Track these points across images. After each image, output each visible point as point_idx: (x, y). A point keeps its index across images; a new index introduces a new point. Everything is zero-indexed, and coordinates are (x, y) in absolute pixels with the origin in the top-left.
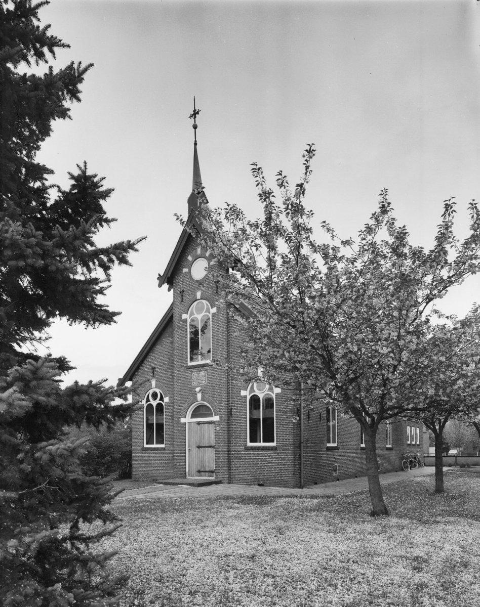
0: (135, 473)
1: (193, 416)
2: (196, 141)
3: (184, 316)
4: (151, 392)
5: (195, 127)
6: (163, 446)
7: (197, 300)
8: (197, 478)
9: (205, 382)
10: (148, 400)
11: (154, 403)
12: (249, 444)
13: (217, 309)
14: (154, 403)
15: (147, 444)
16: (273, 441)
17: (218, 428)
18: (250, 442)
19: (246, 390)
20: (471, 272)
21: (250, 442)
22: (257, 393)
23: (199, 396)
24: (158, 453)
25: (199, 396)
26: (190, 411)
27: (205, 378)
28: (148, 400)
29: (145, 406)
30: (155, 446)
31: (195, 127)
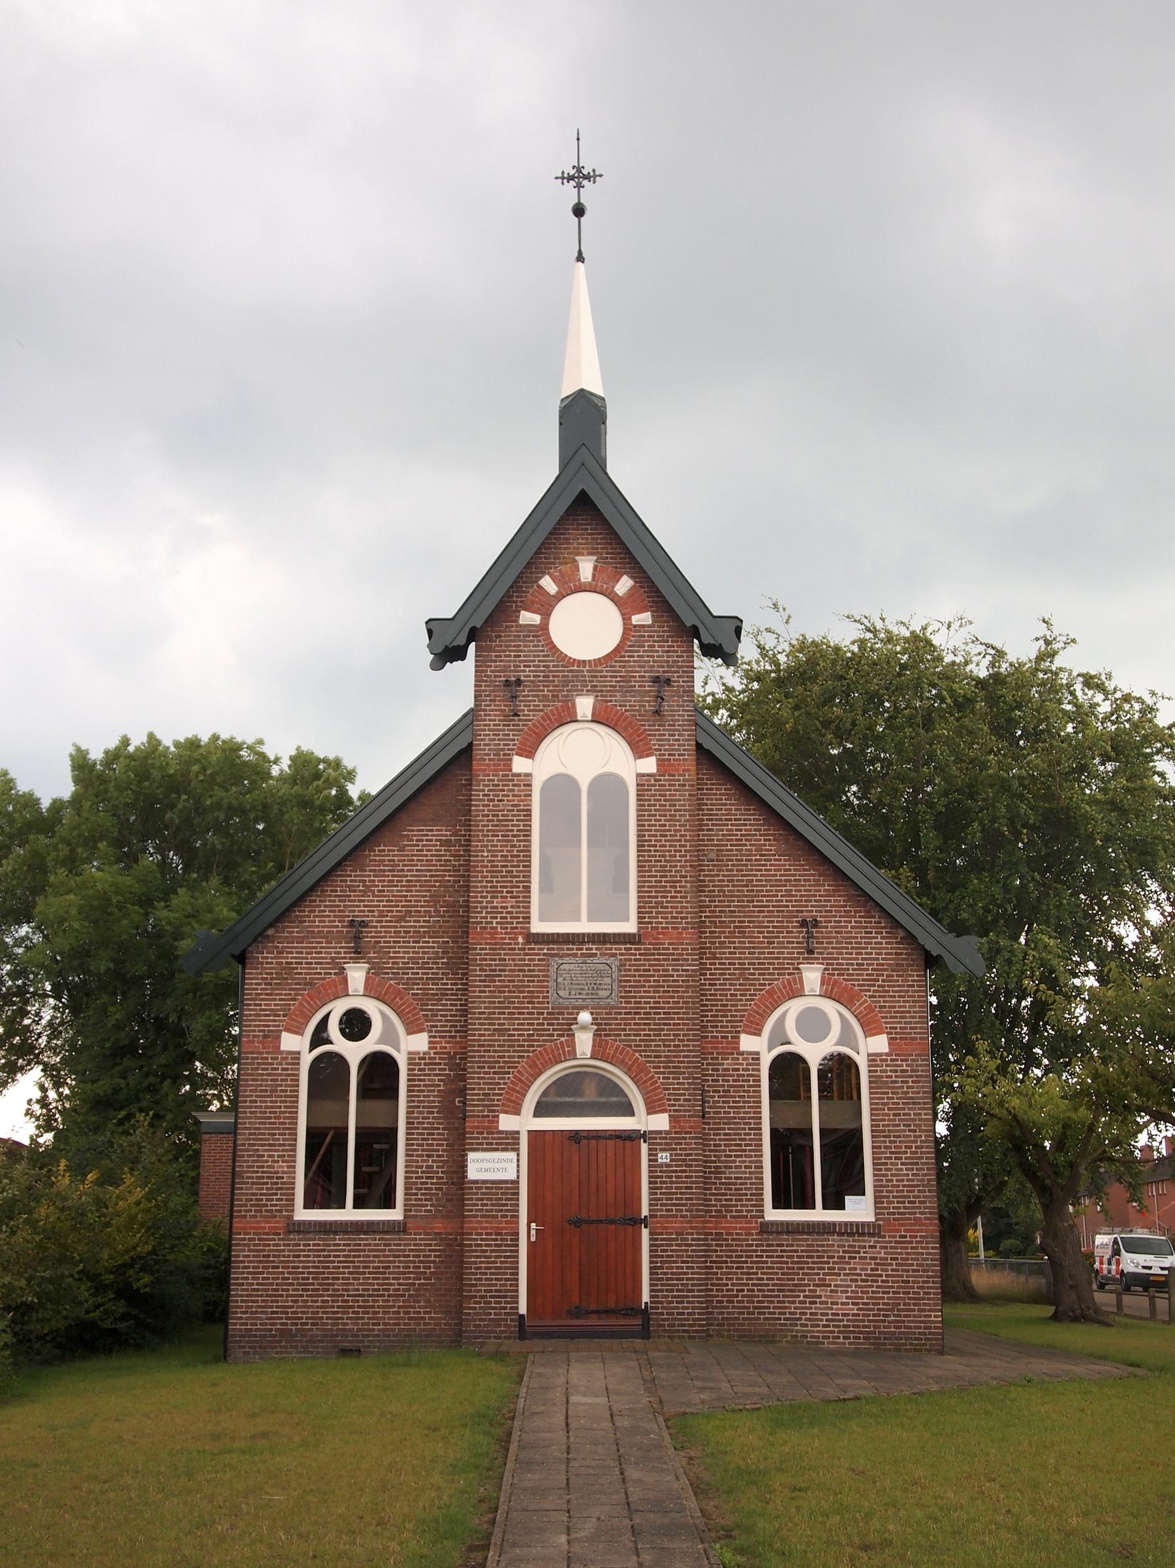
0: (239, 1321)
1: (541, 1110)
2: (580, 252)
3: (520, 764)
4: (338, 1009)
5: (579, 211)
6: (394, 1215)
7: (577, 721)
8: (568, 1322)
9: (609, 993)
10: (320, 1037)
11: (354, 1052)
12: (774, 1215)
13: (658, 765)
14: (354, 1052)
15: (308, 1205)
16: (389, 1203)
17: (664, 1157)
18: (305, 1207)
19: (758, 1033)
20: (1051, 1310)
21: (305, 1207)
22: (800, 1046)
23: (584, 1042)
24: (374, 1240)
25: (584, 1042)
26: (534, 1094)
27: (608, 981)
28: (320, 1037)
29: (307, 1059)
30: (349, 1214)
31: (579, 211)
